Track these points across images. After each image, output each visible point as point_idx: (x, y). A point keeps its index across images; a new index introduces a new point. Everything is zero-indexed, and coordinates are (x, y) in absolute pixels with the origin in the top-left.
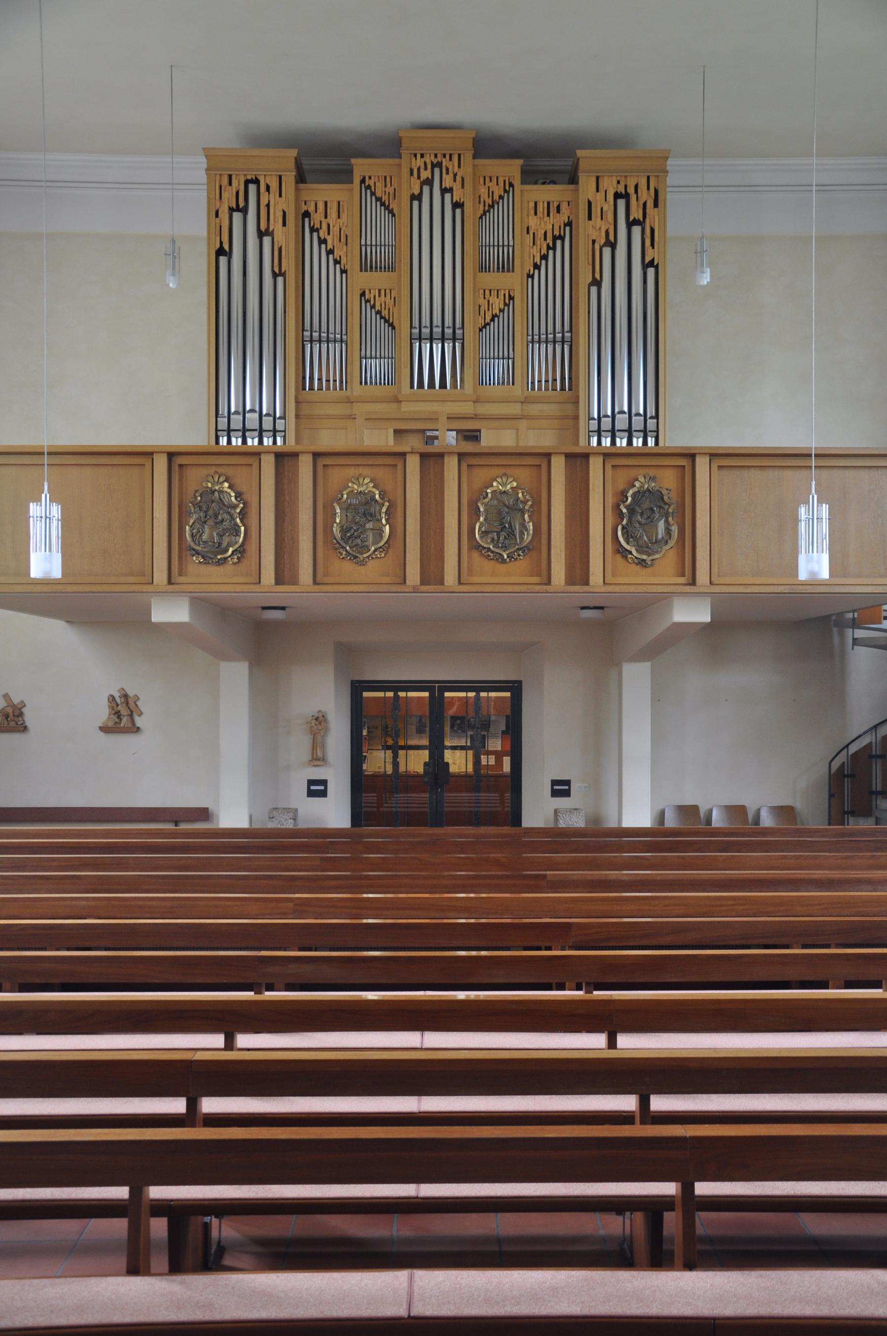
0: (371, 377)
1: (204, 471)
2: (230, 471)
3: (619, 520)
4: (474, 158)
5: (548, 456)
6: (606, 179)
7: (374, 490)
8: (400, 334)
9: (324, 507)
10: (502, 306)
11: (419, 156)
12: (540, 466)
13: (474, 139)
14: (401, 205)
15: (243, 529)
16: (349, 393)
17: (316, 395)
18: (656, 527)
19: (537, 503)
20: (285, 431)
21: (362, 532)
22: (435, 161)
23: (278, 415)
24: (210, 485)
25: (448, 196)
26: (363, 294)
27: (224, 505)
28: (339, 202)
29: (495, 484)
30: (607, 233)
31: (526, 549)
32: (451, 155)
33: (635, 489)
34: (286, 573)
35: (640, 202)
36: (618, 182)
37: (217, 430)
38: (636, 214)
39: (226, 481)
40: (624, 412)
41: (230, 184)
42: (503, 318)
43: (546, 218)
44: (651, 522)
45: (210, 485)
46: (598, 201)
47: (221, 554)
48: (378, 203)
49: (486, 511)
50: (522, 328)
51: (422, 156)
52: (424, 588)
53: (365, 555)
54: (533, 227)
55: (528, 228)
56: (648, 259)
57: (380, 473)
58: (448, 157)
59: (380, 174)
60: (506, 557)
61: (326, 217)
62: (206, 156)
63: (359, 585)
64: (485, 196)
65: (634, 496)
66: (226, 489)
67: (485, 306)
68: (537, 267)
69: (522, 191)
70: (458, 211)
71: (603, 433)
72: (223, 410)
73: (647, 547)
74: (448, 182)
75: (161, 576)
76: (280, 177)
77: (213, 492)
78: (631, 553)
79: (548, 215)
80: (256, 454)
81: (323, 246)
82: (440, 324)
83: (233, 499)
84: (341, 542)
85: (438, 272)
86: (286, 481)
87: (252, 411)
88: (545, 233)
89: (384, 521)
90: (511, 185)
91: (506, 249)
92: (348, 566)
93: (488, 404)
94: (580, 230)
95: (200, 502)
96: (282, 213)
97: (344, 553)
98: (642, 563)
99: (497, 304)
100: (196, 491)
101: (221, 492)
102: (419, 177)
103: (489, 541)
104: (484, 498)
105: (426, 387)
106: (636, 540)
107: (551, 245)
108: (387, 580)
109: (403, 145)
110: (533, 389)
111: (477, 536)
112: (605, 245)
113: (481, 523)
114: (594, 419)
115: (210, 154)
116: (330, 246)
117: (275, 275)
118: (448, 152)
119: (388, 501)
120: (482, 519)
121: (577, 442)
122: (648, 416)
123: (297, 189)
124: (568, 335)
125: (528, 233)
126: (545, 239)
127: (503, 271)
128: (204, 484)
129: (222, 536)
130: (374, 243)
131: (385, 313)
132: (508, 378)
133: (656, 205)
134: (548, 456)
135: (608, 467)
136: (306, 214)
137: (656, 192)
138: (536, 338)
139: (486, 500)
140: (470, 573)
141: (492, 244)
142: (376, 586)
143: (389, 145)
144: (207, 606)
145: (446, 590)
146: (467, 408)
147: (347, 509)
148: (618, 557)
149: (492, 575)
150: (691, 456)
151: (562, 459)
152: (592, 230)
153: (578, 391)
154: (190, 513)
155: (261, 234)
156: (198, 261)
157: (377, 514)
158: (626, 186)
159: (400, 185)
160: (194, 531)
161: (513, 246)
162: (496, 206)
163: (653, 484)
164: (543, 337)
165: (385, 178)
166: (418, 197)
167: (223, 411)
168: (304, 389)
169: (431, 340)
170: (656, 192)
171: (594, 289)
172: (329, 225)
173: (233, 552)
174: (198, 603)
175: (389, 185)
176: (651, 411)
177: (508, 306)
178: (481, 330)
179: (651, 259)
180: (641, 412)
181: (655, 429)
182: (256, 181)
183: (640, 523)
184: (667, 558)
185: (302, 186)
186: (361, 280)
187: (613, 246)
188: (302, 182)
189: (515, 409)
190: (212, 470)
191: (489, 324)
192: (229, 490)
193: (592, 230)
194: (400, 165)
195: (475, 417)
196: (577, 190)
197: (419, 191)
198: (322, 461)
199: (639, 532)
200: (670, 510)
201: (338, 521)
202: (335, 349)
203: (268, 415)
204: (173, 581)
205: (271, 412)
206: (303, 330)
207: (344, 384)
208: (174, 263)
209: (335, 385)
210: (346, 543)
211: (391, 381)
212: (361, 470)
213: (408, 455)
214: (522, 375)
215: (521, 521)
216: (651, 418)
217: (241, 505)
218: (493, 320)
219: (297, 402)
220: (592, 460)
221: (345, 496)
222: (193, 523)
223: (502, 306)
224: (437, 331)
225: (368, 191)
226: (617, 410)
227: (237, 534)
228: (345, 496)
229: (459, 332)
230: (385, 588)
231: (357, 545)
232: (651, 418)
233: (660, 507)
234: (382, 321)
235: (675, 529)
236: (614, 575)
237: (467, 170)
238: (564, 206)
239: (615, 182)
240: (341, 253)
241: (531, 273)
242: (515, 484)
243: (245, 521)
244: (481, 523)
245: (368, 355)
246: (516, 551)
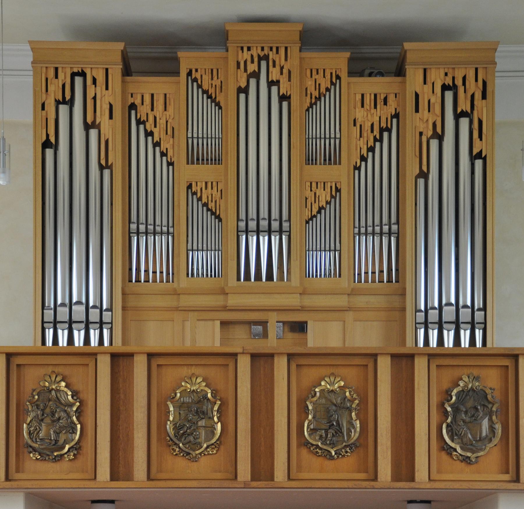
0: (198, 269)
1: (42, 371)
3: (444, 418)
4: (300, 51)
5: (374, 356)
6: (433, 71)
7: (206, 389)
8: (227, 226)
9: (158, 404)
10: (329, 199)
11: (245, 49)
12: (367, 366)
13: (300, 31)
14: (228, 98)
15: (79, 426)
16: (175, 285)
17: (142, 287)
19: (364, 401)
22: (262, 54)
23: (105, 307)
24: (47, 384)
25: (274, 89)
26: (190, 187)
28: (165, 95)
29: (323, 383)
30: (434, 125)
32: (277, 48)
35: (469, 94)
36: (446, 74)
37: (43, 322)
38: (464, 105)
39: (63, 380)
41: (57, 77)
42: (330, 210)
43: (373, 111)
44: (475, 420)
46: (425, 93)
48: (205, 96)
49: (315, 409)
50: (349, 220)
51: (249, 49)
52: (255, 484)
53: (197, 452)
54: (360, 120)
55: (355, 120)
56: (475, 151)
57: (213, 373)
58: (274, 50)
59: (205, 67)
60: (333, 453)
61: (152, 110)
62: (32, 49)
64: (311, 89)
65: (458, 395)
66: (62, 388)
67: (311, 199)
68: (363, 159)
69: (349, 83)
70: (285, 104)
71: (430, 325)
72: (50, 302)
73: (472, 445)
74: (275, 75)
76: (107, 70)
77: (50, 391)
78: (455, 450)
79: (375, 107)
80: (89, 355)
81: (150, 138)
82: (266, 216)
83: (70, 397)
84: (175, 440)
85: (263, 144)
86: (121, 380)
87: (79, 303)
88: (372, 125)
89: (216, 419)
90: (338, 77)
91: (332, 141)
92: (181, 463)
94: (407, 122)
95: (37, 401)
96: (108, 106)
97: (177, 449)
98: (466, 460)
99: (324, 196)
101: (58, 391)
102: (246, 70)
103: (317, 438)
104: (313, 397)
105: (253, 280)
107: (378, 137)
108: (219, 475)
109: (229, 38)
110: (360, 281)
111: (306, 433)
112: (432, 137)
113: (310, 421)
114: (421, 311)
115: (36, 47)
116: (156, 139)
117: (102, 168)
118: (274, 46)
119: (220, 400)
120: (310, 417)
121: (403, 342)
122: (476, 308)
123: (123, 82)
124: (394, 228)
125: (355, 125)
126: (372, 131)
127: (330, 164)
128: (41, 384)
130: (200, 136)
131: (211, 205)
133: (484, 97)
134: (374, 356)
135: (433, 367)
136: (133, 106)
137: (484, 83)
138: (363, 230)
139: (315, 399)
140: (299, 468)
141: (318, 136)
142: (209, 482)
143: (215, 37)
145: (276, 486)
146: (293, 301)
147: (180, 407)
148: (443, 454)
149: (321, 472)
151: (388, 359)
152: (419, 122)
153: (405, 283)
154: (28, 411)
155: (87, 127)
156: (24, 151)
158: (454, 78)
159: (227, 78)
160: (32, 429)
161: (340, 138)
162: (323, 99)
163: (477, 384)
164: (370, 229)
165: (212, 70)
166: (245, 91)
168: (131, 281)
169: (258, 232)
170: (484, 83)
171: (421, 181)
172: (155, 118)
175: (215, 78)
177: (335, 198)
178: (307, 222)
179: (478, 150)
180: (469, 303)
181: (483, 321)
182: (83, 74)
183: (464, 421)
184: (491, 456)
185: (128, 78)
186: (187, 172)
187: (440, 138)
188: (128, 75)
189: (341, 301)
190: (50, 369)
191: (315, 216)
192: (66, 389)
193: (419, 122)
194: (227, 58)
195: (302, 309)
196: (404, 82)
197: (246, 84)
198: (155, 362)
200: (494, 409)
201: (171, 418)
202: (161, 241)
203: (94, 307)
204: (10, 478)
205: (98, 304)
206: (130, 222)
208: (4, 159)
210: (180, 440)
211: (216, 274)
216: (479, 310)
217: (78, 404)
218: (319, 212)
219: (124, 294)
220: (417, 360)
221: (178, 395)
222: (31, 421)
223: (329, 199)
224: (264, 224)
225: (195, 84)
226: (444, 302)
228: (178, 395)
229: (285, 225)
230: (217, 484)
232: (479, 310)
233: (484, 406)
234: (209, 213)
235: (498, 427)
236: (439, 471)
237: (293, 63)
238: (391, 99)
239: (442, 75)
240: (168, 146)
241: (358, 165)
242: (342, 384)
243: (81, 419)
244: (310, 421)
245: (195, 247)
246: (343, 448)
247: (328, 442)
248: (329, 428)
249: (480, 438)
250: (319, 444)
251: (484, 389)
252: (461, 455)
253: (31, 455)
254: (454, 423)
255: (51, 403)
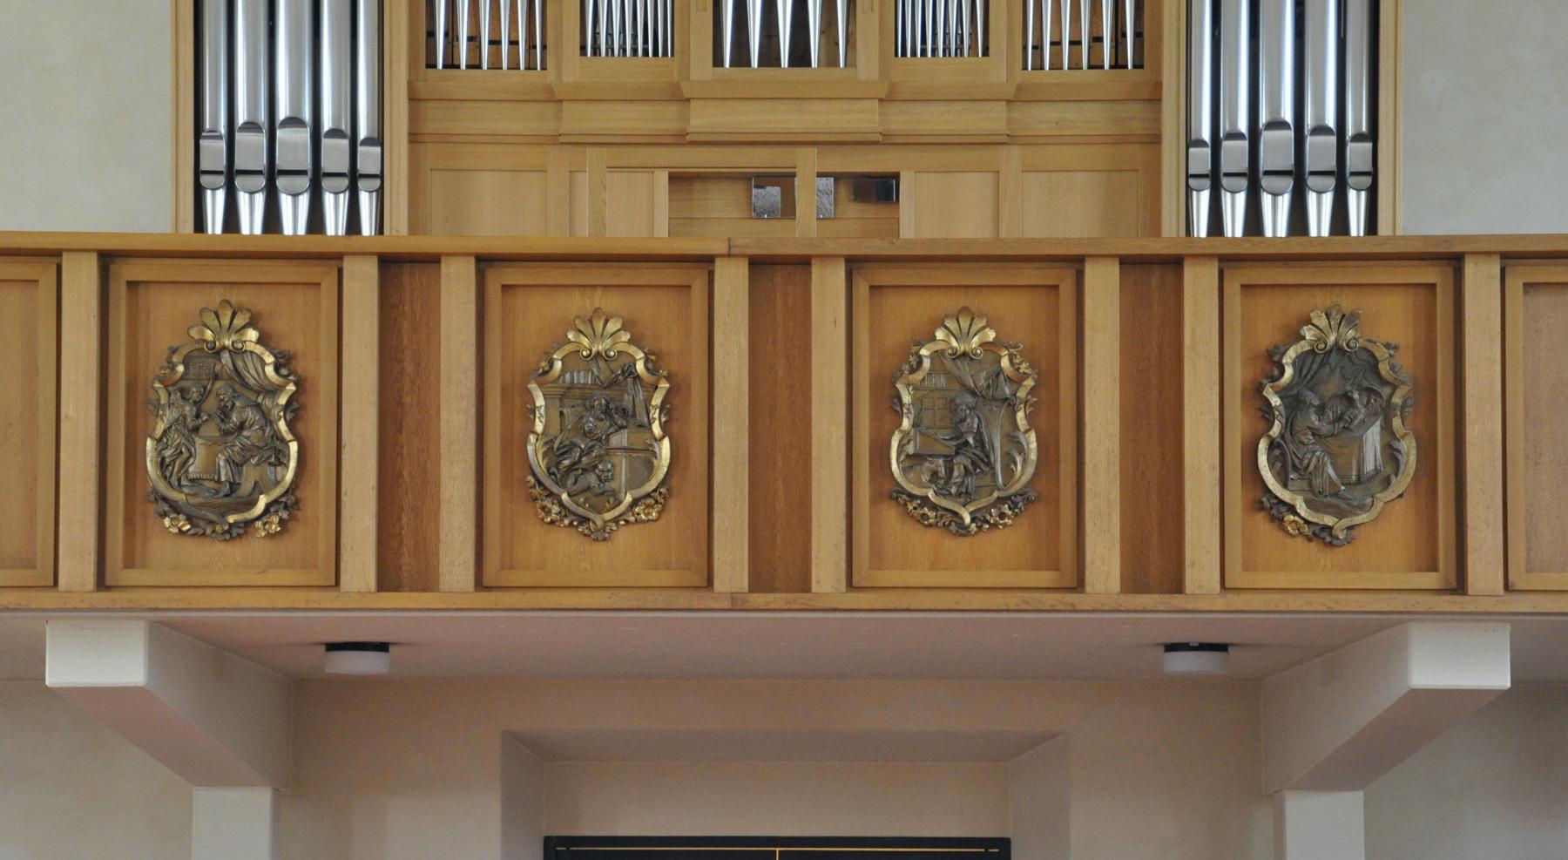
0: (610, 34)
1: (195, 301)
2: (261, 301)
3: (1262, 425)
5: (1076, 263)
7: (632, 350)
9: (503, 390)
12: (1056, 287)
15: (294, 447)
18: (1360, 442)
20: (381, 176)
21: (600, 458)
23: (363, 133)
24: (209, 335)
27: (245, 385)
29: (940, 334)
31: (1019, 501)
33: (1302, 347)
34: (405, 560)
37: (198, 172)
39: (252, 324)
40: (1282, 125)
44: (1345, 427)
45: (209, 335)
47: (237, 511)
49: (918, 402)
52: (759, 599)
57: (649, 307)
60: (967, 520)
63: (598, 583)
65: (1299, 363)
66: (250, 347)
71: (1225, 181)
75: (77, 567)
77: (217, 353)
78: (1292, 509)
83: (270, 370)
84: (548, 482)
86: (406, 326)
87: (294, 121)
89: (656, 429)
92: (565, 544)
93: (919, 107)
95: (184, 377)
97: (555, 509)
98: (1322, 535)
100: (174, 351)
101: (237, 352)
103: (925, 478)
104: (913, 371)
106: (1303, 472)
108: (664, 578)
110: (1039, 66)
113: (906, 434)
114: (1201, 143)
119: (669, 378)
120: (906, 423)
121: (1154, 227)
122: (1350, 132)
128: (194, 333)
129: (239, 466)
132: (973, 35)
134: (1076, 263)
139: (919, 376)
144: (204, 652)
146: (862, 118)
147: (562, 397)
148: (1260, 519)
149: (933, 567)
150: (1453, 260)
151: (1114, 269)
154: (158, 406)
157: (640, 410)
160: (168, 453)
163: (1351, 333)
167: (215, 120)
168: (432, 65)
173: (268, 506)
174: (175, 639)
176: (1357, 120)
180: (1331, 121)
181: (1369, 168)
183: (1315, 433)
184: (1388, 524)
189: (992, 119)
190: (216, 296)
192: (259, 349)
195: (885, 141)
199: (1315, 455)
201: (539, 427)
203: (335, 133)
205: (345, 126)
207: (538, 51)
209: (513, 55)
210: (561, 483)
212: (599, 300)
213: (718, 262)
214: (1010, 31)
215: (1008, 428)
216: (1358, 137)
217: (291, 388)
219: (413, 99)
220: (1190, 272)
221: (558, 365)
222: (165, 432)
226: (1263, 118)
227: (280, 460)
228: (558, 365)
230: (660, 599)
231: (589, 488)
232: (1358, 137)
233: (1370, 391)
235: (1408, 448)
236: (1248, 566)
243: (300, 427)
246: (993, 505)
247: (953, 490)
248: (957, 453)
249: (1359, 477)
250: (931, 494)
251: (1369, 346)
252: (1307, 522)
253: (167, 522)
254: (1287, 435)
255: (219, 384)
